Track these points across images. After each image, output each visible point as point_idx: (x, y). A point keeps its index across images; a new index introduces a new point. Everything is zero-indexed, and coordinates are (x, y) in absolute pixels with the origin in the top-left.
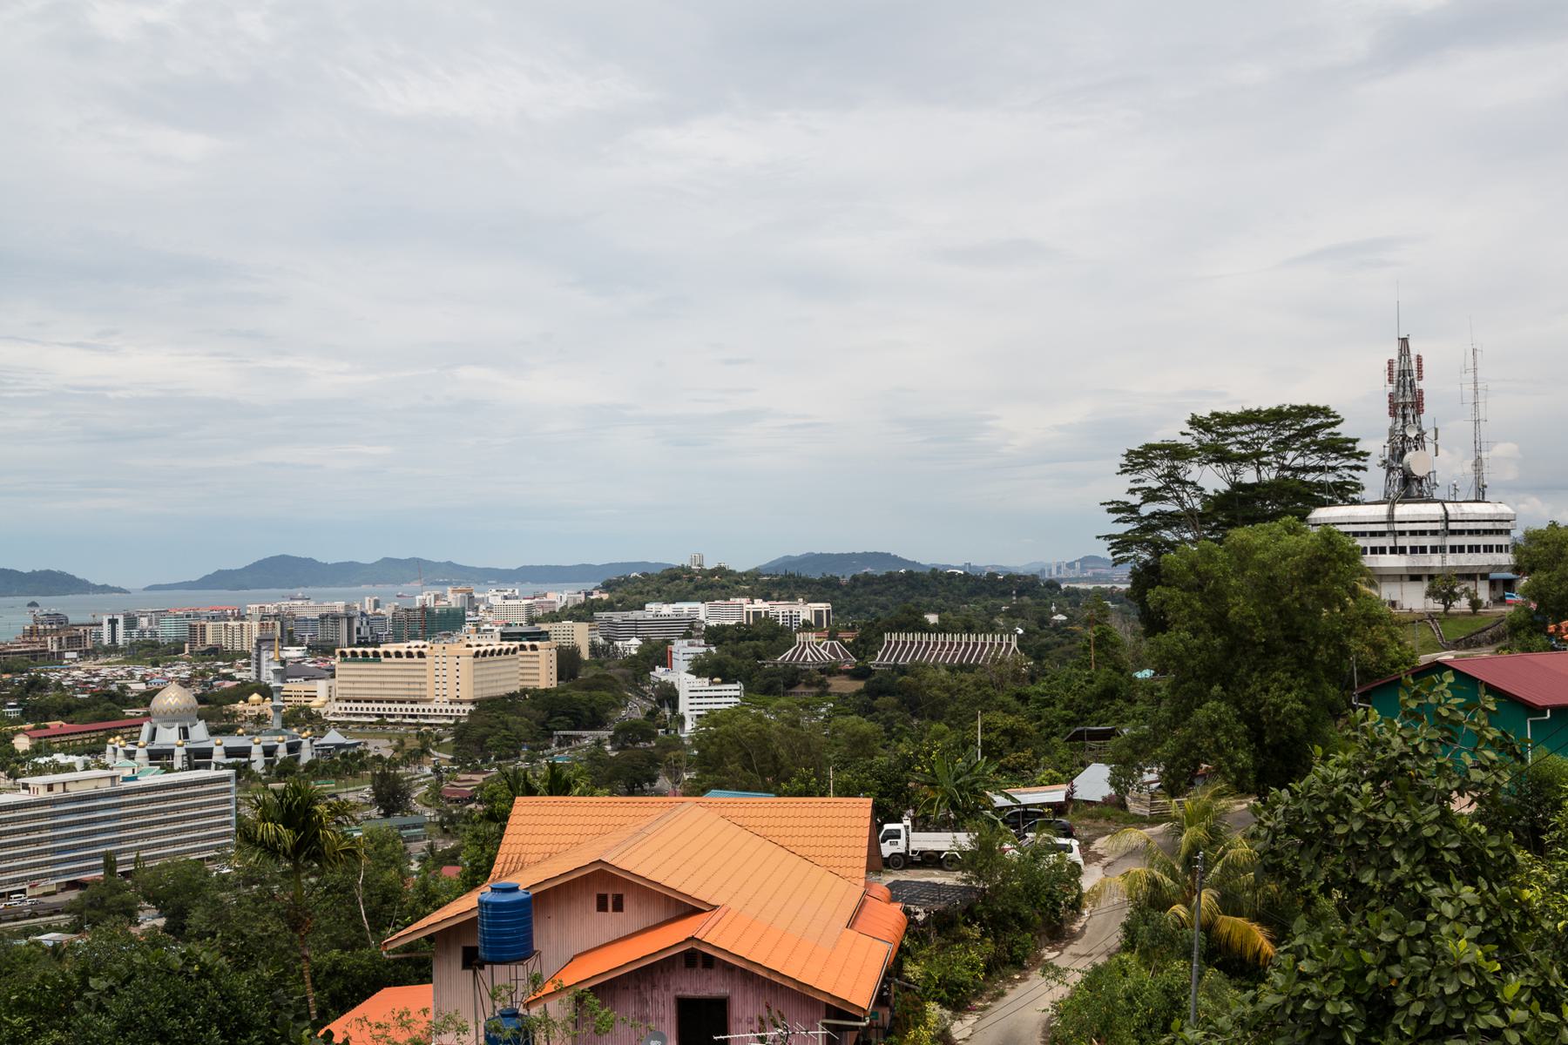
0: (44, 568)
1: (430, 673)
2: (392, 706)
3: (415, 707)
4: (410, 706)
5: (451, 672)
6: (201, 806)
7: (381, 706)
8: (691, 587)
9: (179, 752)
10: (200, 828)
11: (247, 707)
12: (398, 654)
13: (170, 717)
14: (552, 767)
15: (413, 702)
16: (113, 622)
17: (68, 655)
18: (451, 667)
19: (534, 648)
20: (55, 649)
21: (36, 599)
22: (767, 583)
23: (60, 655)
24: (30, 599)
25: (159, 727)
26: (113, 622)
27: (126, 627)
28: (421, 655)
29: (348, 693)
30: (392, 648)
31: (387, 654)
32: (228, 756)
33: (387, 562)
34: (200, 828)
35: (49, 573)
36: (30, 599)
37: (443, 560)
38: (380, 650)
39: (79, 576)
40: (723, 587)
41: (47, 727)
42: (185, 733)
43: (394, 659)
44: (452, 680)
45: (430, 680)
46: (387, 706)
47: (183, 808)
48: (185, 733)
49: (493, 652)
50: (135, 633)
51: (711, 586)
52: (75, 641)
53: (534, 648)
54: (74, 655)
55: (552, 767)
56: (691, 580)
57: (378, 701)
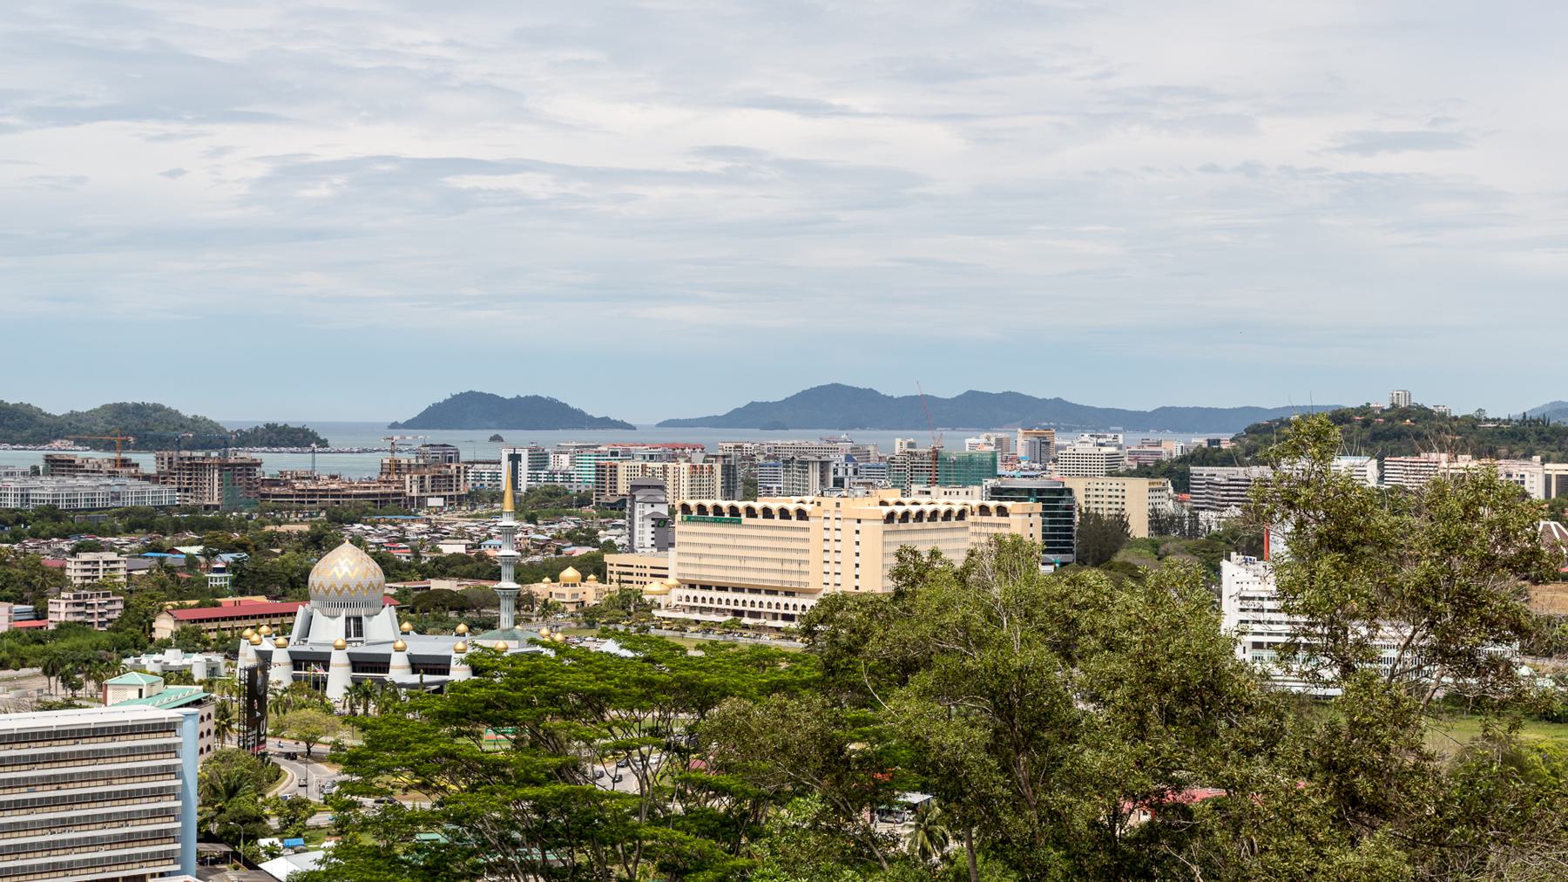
0: (530, 394)
1: (815, 545)
2: (757, 598)
3: (791, 601)
4: (783, 600)
5: (848, 548)
6: (108, 777)
7: (740, 597)
8: (1366, 434)
9: (339, 660)
10: (107, 819)
11: (556, 588)
12: (784, 514)
13: (338, 599)
14: (267, 817)
15: (789, 593)
16: (515, 459)
17: (432, 502)
18: (848, 535)
19: (1002, 511)
20: (415, 493)
21: (501, 433)
22: (1491, 433)
23: (421, 502)
24: (493, 433)
25: (317, 614)
26: (515, 459)
27: (531, 468)
28: (802, 515)
29: (693, 573)
30: (775, 504)
31: (767, 513)
32: (414, 671)
33: (972, 397)
34: (107, 819)
35: (537, 400)
36: (493, 433)
37: (1050, 396)
38: (757, 505)
39: (573, 404)
40: (1418, 436)
41: (217, 605)
42: (356, 627)
43: (777, 521)
44: (848, 559)
45: (815, 557)
46: (749, 597)
47: (70, 779)
48: (356, 627)
49: (905, 517)
50: (543, 474)
51: (1399, 435)
52: (442, 482)
53: (1002, 511)
54: (439, 502)
55: (267, 817)
56: (1366, 424)
57: (737, 589)
